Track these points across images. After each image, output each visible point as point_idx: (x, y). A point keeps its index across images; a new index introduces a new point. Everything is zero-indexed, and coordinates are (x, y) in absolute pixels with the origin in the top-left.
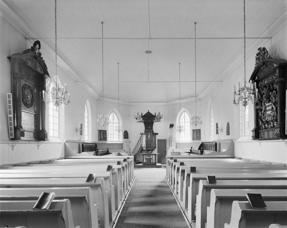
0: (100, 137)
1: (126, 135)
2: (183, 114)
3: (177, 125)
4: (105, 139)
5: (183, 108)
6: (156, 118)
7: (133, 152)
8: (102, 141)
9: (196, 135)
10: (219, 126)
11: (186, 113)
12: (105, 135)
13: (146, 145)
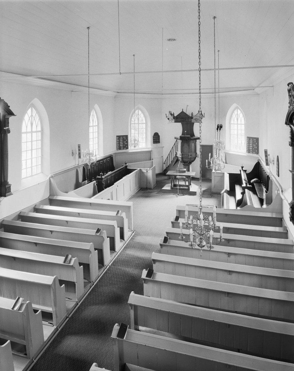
0: (118, 145)
1: (156, 138)
2: (236, 112)
3: (226, 127)
4: (126, 147)
5: (235, 104)
6: (193, 119)
7: (165, 163)
8: (122, 150)
9: (253, 145)
10: (268, 153)
11: (239, 111)
12: (126, 141)
13: (182, 154)
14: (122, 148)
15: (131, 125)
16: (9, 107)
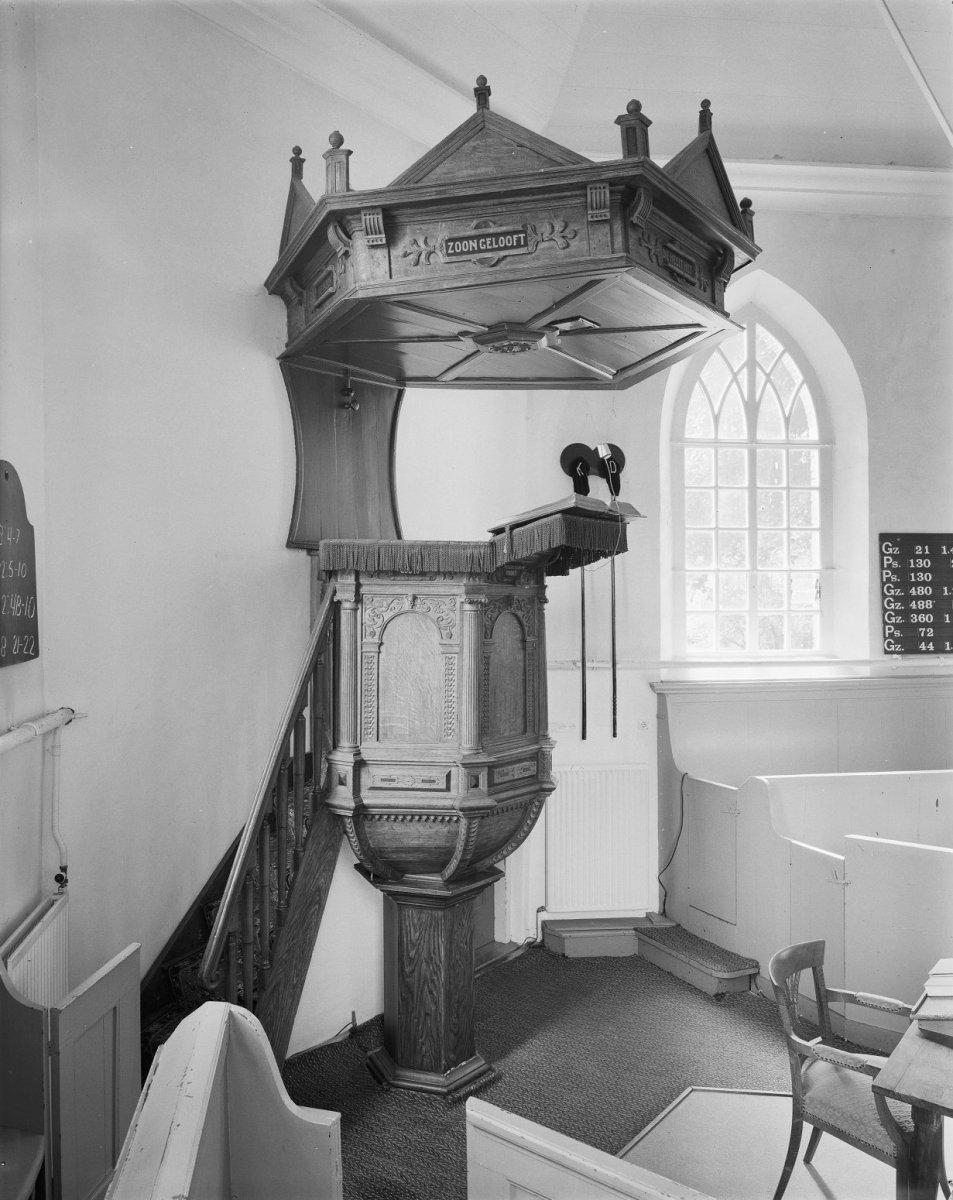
0: (897, 613)
14: (927, 640)
15: (677, 456)
16: (546, 601)
